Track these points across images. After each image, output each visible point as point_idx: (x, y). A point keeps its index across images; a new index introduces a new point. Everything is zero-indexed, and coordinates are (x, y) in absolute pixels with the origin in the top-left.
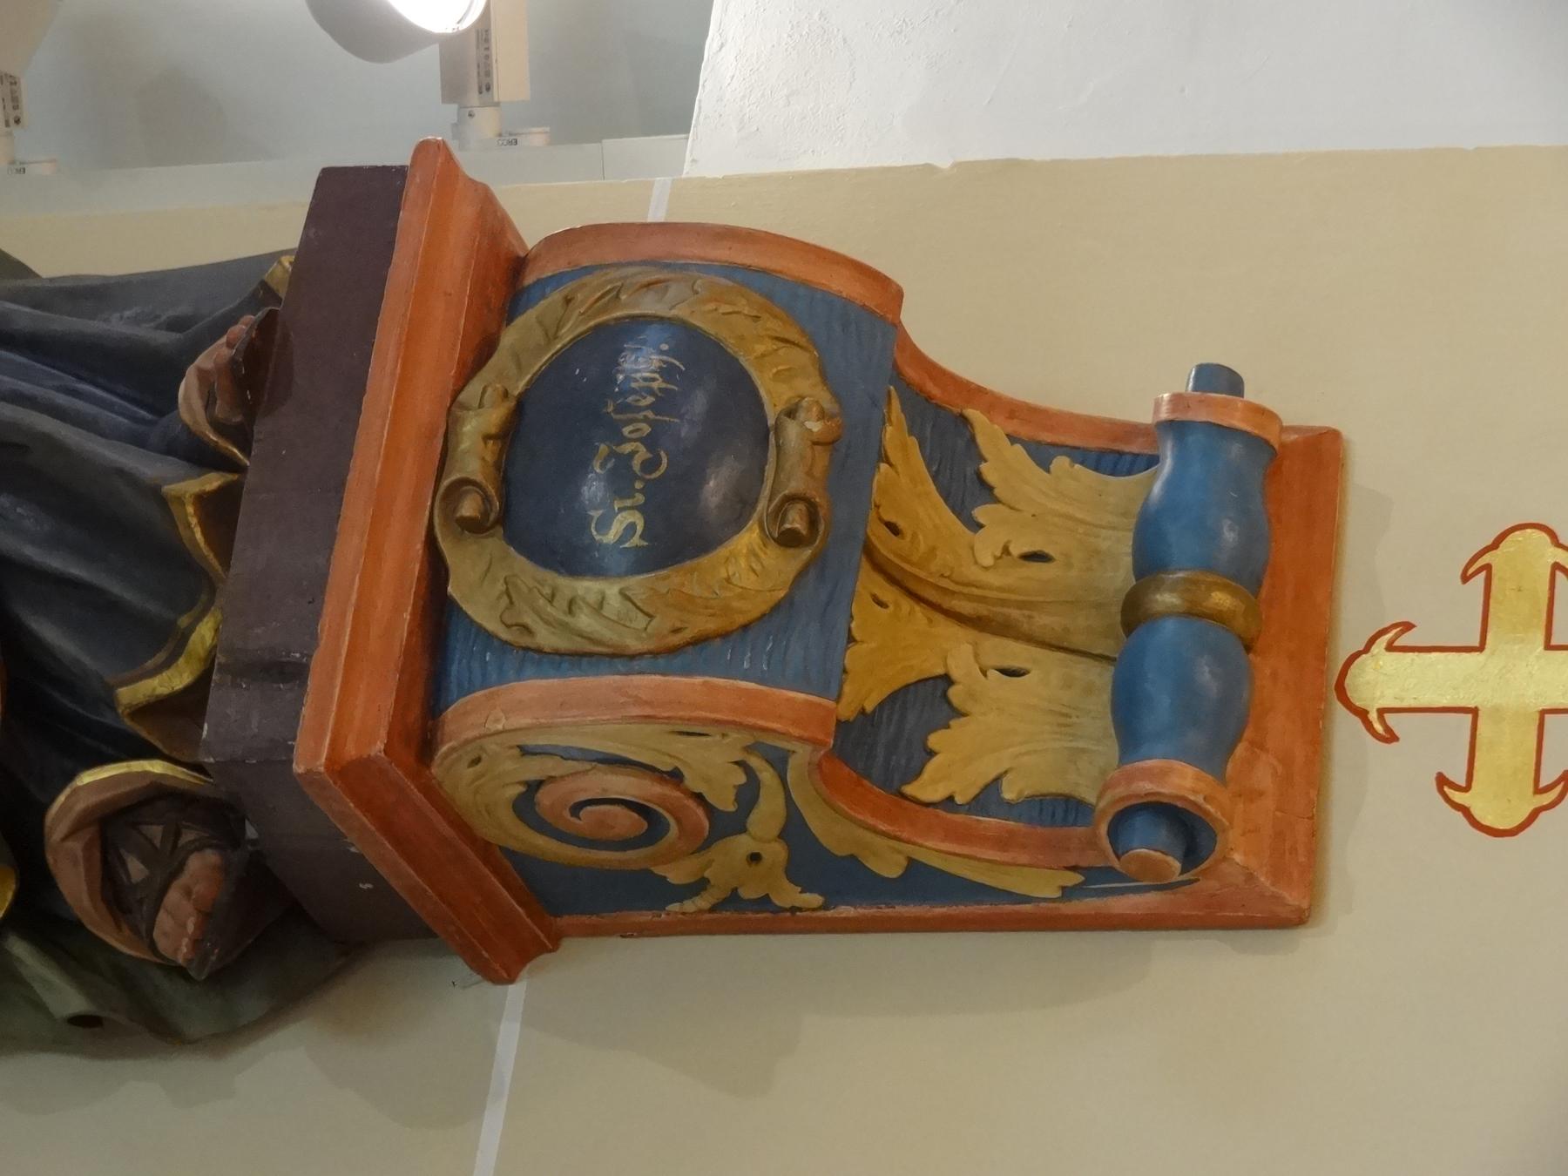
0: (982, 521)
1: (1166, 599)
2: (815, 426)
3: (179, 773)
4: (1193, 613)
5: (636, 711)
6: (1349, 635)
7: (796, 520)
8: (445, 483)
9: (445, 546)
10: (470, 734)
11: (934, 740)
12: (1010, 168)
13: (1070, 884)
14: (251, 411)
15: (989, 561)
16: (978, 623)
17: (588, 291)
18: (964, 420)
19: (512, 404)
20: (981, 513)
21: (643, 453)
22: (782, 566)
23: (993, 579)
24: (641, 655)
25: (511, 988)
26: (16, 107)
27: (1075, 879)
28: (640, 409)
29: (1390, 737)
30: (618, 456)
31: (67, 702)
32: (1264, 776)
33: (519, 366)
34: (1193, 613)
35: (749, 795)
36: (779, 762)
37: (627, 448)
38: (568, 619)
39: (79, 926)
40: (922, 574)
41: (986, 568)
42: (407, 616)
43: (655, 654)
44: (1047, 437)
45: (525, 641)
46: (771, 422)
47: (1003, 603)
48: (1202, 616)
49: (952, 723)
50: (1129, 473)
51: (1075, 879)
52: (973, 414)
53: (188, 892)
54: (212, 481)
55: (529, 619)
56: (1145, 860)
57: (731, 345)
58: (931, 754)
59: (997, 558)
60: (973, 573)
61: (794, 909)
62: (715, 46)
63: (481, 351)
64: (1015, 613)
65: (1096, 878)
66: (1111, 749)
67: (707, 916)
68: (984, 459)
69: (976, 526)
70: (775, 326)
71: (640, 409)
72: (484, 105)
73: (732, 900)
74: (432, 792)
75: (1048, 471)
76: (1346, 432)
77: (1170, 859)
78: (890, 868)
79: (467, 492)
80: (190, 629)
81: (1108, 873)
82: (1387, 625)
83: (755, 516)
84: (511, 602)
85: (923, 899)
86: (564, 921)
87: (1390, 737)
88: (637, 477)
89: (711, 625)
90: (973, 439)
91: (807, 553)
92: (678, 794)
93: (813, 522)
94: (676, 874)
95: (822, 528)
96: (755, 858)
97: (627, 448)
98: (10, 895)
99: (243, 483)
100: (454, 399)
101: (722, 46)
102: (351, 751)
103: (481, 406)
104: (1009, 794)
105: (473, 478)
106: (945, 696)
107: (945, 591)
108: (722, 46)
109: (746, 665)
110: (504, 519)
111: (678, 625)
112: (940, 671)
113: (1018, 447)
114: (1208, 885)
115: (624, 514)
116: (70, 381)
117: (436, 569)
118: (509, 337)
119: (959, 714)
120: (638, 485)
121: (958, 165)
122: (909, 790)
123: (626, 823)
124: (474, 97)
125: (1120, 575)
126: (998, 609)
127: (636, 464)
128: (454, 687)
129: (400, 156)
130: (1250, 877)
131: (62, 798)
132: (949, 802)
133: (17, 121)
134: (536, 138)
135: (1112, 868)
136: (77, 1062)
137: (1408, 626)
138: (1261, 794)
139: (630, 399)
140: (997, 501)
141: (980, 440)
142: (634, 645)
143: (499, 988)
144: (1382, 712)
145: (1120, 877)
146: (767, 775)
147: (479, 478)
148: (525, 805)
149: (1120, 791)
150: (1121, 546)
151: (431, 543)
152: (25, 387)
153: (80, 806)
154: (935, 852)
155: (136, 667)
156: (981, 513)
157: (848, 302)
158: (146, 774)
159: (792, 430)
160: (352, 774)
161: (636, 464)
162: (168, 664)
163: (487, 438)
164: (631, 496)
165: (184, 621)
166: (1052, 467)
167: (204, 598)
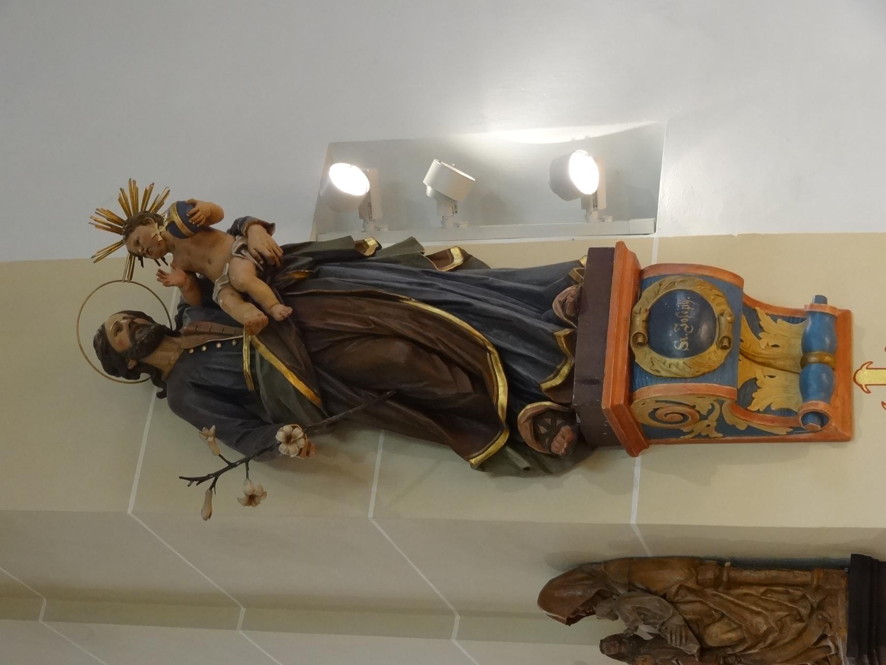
0: (761, 337)
1: (813, 359)
2: (729, 318)
3: (555, 405)
4: (821, 362)
5: (689, 392)
6: (856, 365)
7: (726, 343)
8: (633, 335)
9: (634, 349)
10: (645, 398)
11: (754, 395)
12: (754, 236)
13: (789, 431)
14: (577, 314)
15: (764, 348)
16: (763, 364)
17: (667, 281)
18: (755, 310)
19: (648, 312)
20: (761, 335)
21: (687, 327)
22: (722, 354)
23: (764, 352)
24: (688, 378)
25: (637, 458)
26: (456, 208)
27: (791, 430)
28: (685, 315)
29: (869, 392)
30: (681, 327)
31: (521, 386)
32: (838, 403)
33: (648, 303)
34: (821, 362)
35: (710, 412)
36: (721, 403)
37: (682, 325)
38: (670, 369)
39: (525, 444)
40: (748, 352)
41: (763, 349)
42: (626, 368)
43: (692, 378)
44: (775, 314)
45: (658, 374)
46: (716, 317)
47: (767, 358)
48: (824, 363)
49: (758, 390)
50: (797, 323)
51: (791, 430)
52: (757, 308)
53: (563, 437)
54: (567, 331)
55: (659, 369)
56: (812, 426)
57: (705, 297)
58: (753, 398)
59: (765, 347)
60: (760, 351)
61: (714, 438)
62: (662, 196)
63: (636, 298)
64: (772, 361)
65: (797, 429)
66: (799, 397)
67: (691, 439)
68: (760, 320)
69: (760, 338)
70: (716, 292)
71: (685, 315)
72: (594, 211)
73: (699, 435)
74: (630, 411)
75: (776, 322)
76: (852, 311)
77: (818, 426)
78: (742, 427)
79: (640, 336)
80: (561, 369)
81: (801, 429)
82: (866, 362)
83: (715, 342)
84: (653, 364)
85: (753, 435)
86: (652, 441)
87: (869, 392)
88: (685, 333)
89: (707, 370)
90: (757, 316)
91: (728, 351)
92: (694, 411)
93: (730, 343)
94: (685, 430)
95: (732, 345)
96: (708, 426)
97: (682, 325)
98: (507, 437)
99: (576, 334)
100: (632, 310)
101: (664, 196)
102: (616, 403)
103: (640, 313)
104: (773, 409)
105: (640, 332)
106: (755, 383)
107: (754, 356)
108: (664, 196)
109: (715, 380)
110: (649, 342)
111: (698, 370)
112: (754, 377)
113: (769, 317)
114: (825, 431)
115: (684, 342)
116: (514, 300)
117: (631, 356)
118: (644, 294)
119: (759, 388)
120: (686, 335)
121: (739, 235)
122: (749, 408)
123: (679, 418)
124: (592, 209)
125: (798, 351)
126: (767, 360)
127: (685, 329)
128: (637, 386)
129: (613, 246)
130: (836, 429)
131: (522, 412)
132: (758, 411)
133: (456, 212)
134: (609, 219)
135: (801, 428)
136: (520, 479)
137: (871, 363)
138: (838, 408)
139: (682, 312)
140: (764, 331)
141: (759, 315)
142: (688, 376)
143: (634, 458)
144: (866, 385)
145: (803, 429)
146: (717, 406)
147: (643, 332)
148: (653, 415)
149: (806, 409)
150: (798, 343)
151: (630, 348)
152: (504, 303)
153: (529, 414)
154: (756, 424)
155: (545, 376)
156: (761, 335)
157: (731, 284)
158: (545, 405)
159: (723, 319)
160: (615, 408)
161: (685, 329)
162: (555, 377)
163: (643, 321)
164: (684, 338)
165: (558, 367)
166: (777, 322)
167: (563, 361)
